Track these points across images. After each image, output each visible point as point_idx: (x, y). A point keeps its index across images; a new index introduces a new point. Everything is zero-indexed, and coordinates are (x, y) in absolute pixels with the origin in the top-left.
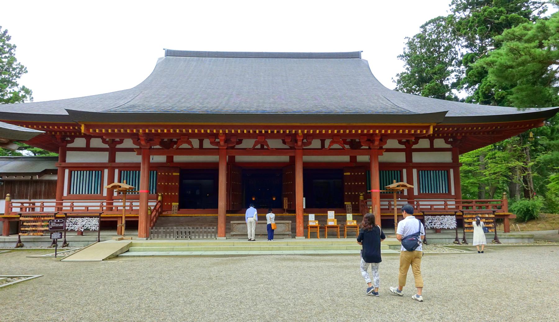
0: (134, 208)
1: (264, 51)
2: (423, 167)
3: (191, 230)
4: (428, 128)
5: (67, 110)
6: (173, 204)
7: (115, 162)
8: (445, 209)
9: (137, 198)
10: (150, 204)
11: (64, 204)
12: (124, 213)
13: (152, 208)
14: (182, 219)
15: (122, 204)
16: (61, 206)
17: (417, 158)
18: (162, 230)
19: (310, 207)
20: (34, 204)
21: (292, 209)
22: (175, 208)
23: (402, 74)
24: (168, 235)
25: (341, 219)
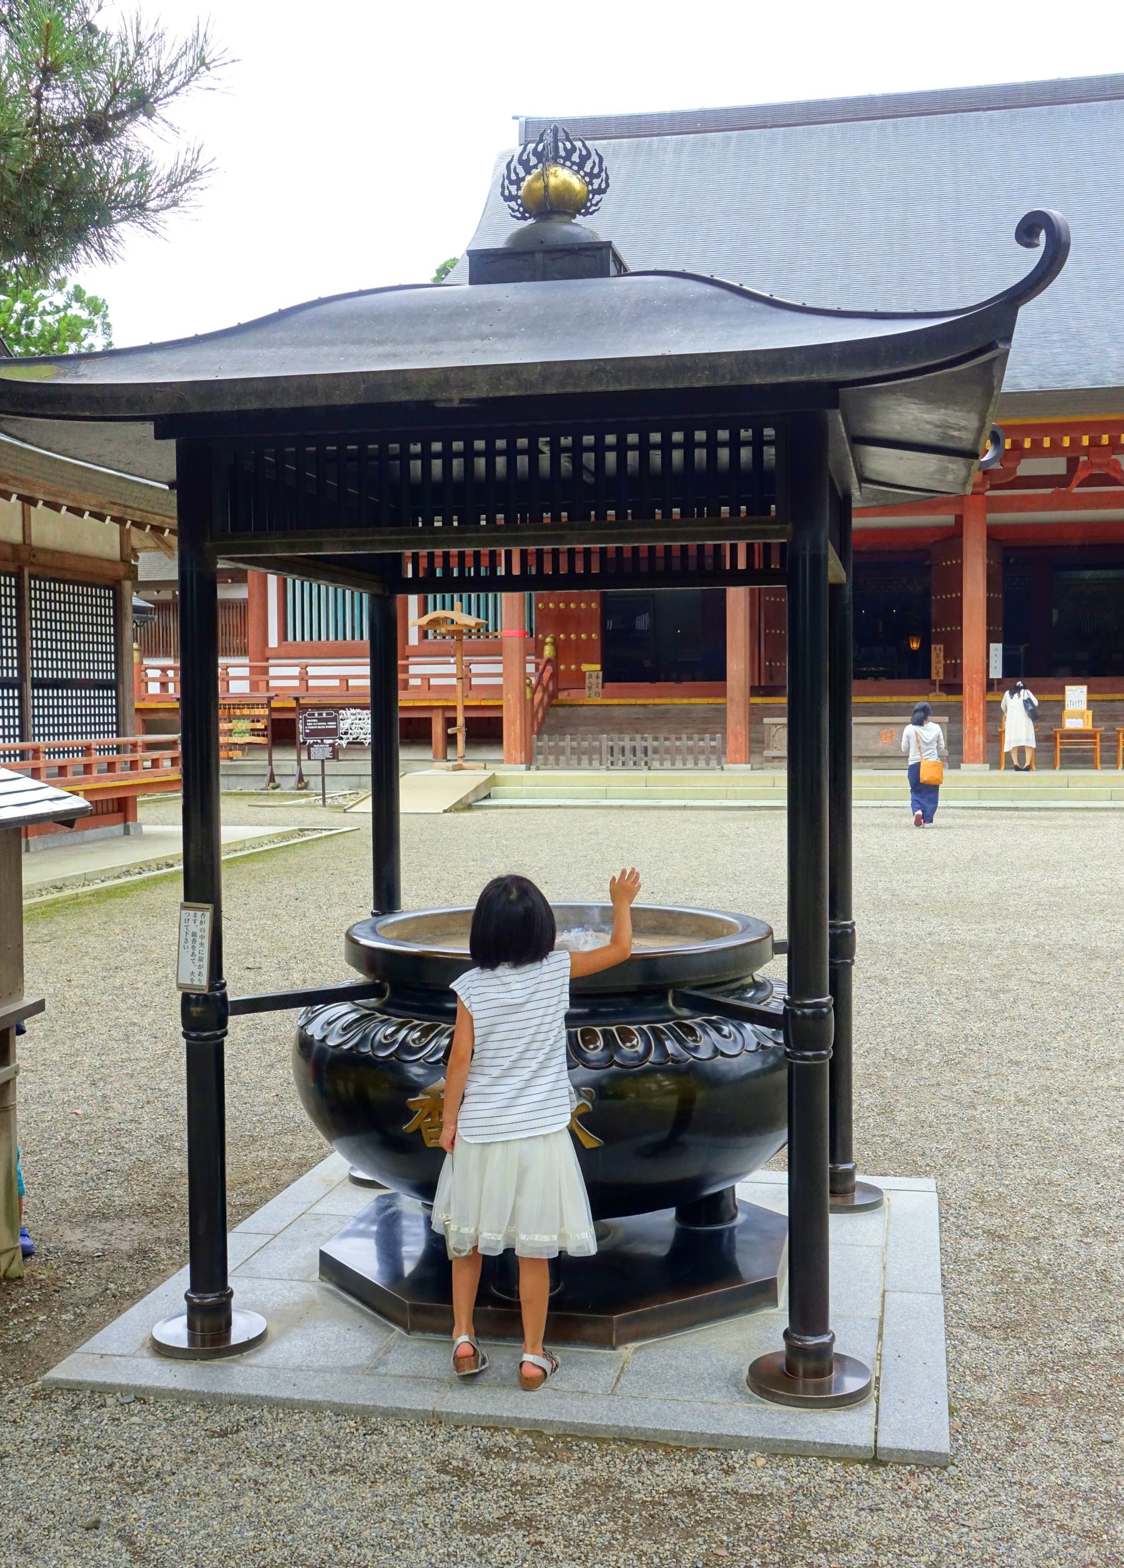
0: (311, 683)
3: (651, 744)
6: (585, 667)
11: (273, 671)
12: (459, 694)
14: (617, 712)
15: (296, 671)
18: (567, 742)
19: (1020, 669)
21: (953, 681)
22: (594, 680)
24: (585, 758)
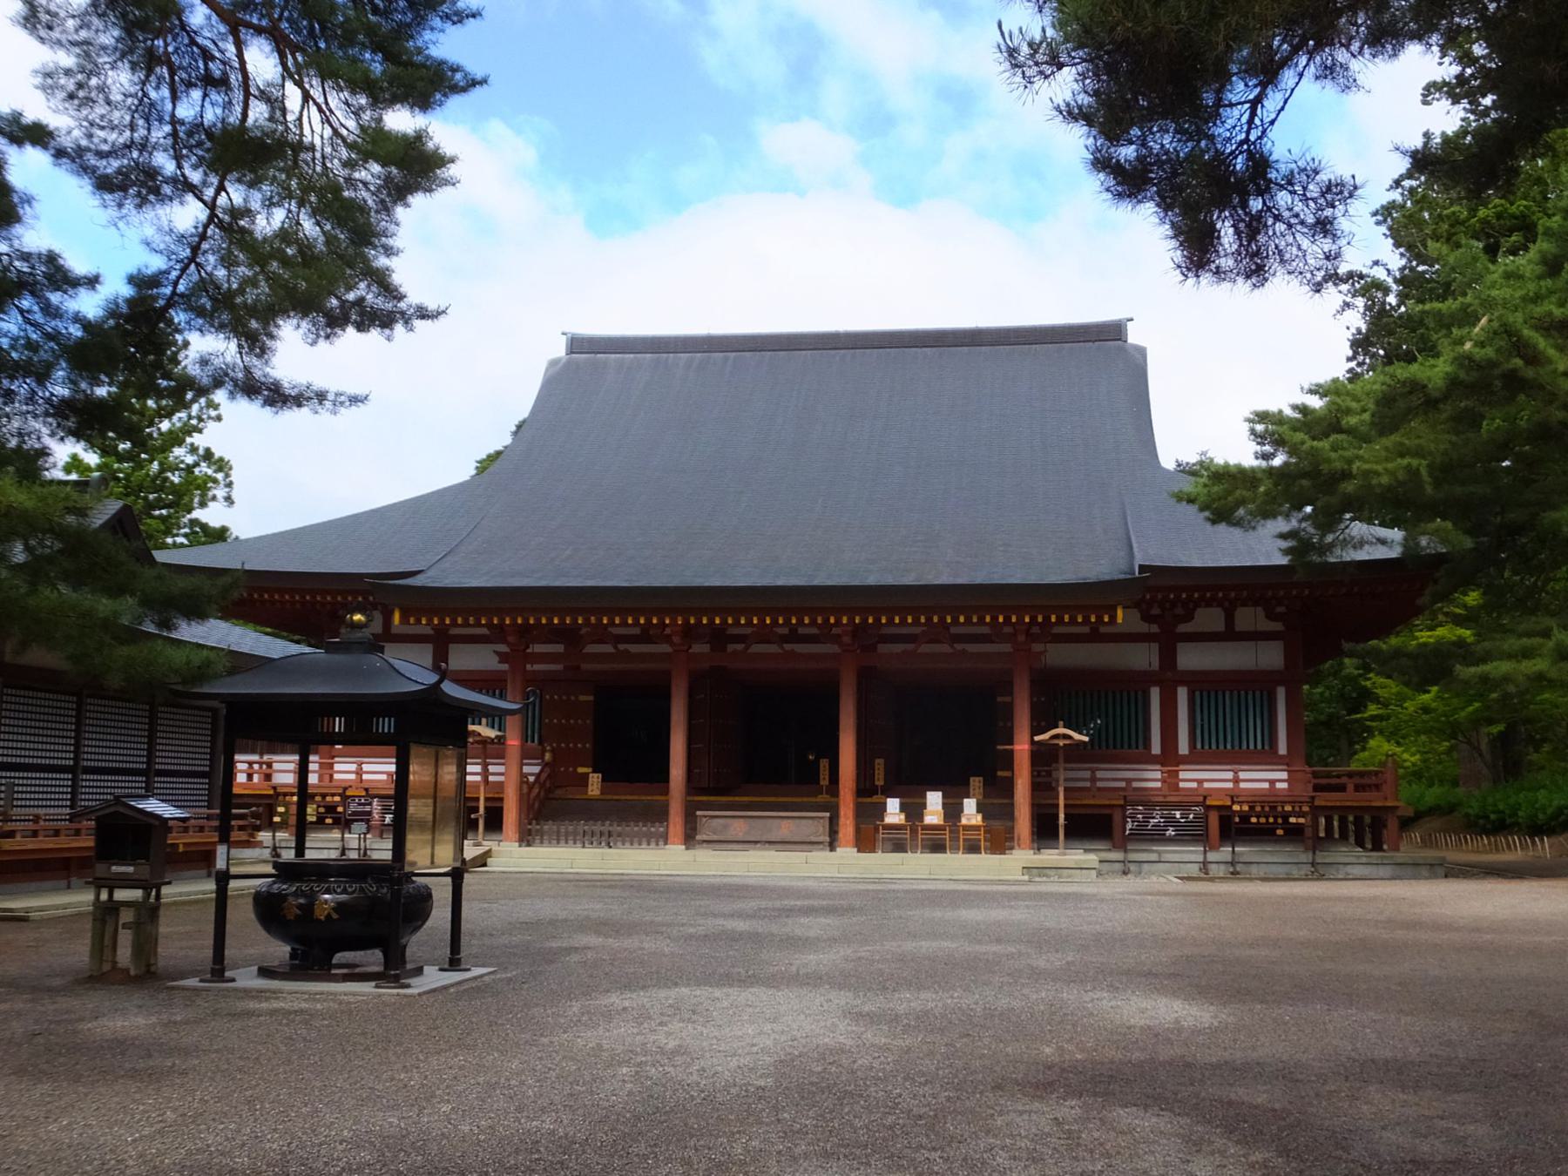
0: (491, 778)
1: (270, 532)
2: (1206, 686)
9: (501, 755)
10: (526, 769)
11: (337, 767)
13: (532, 779)
17: (1191, 658)
20: (269, 765)
25: (952, 811)
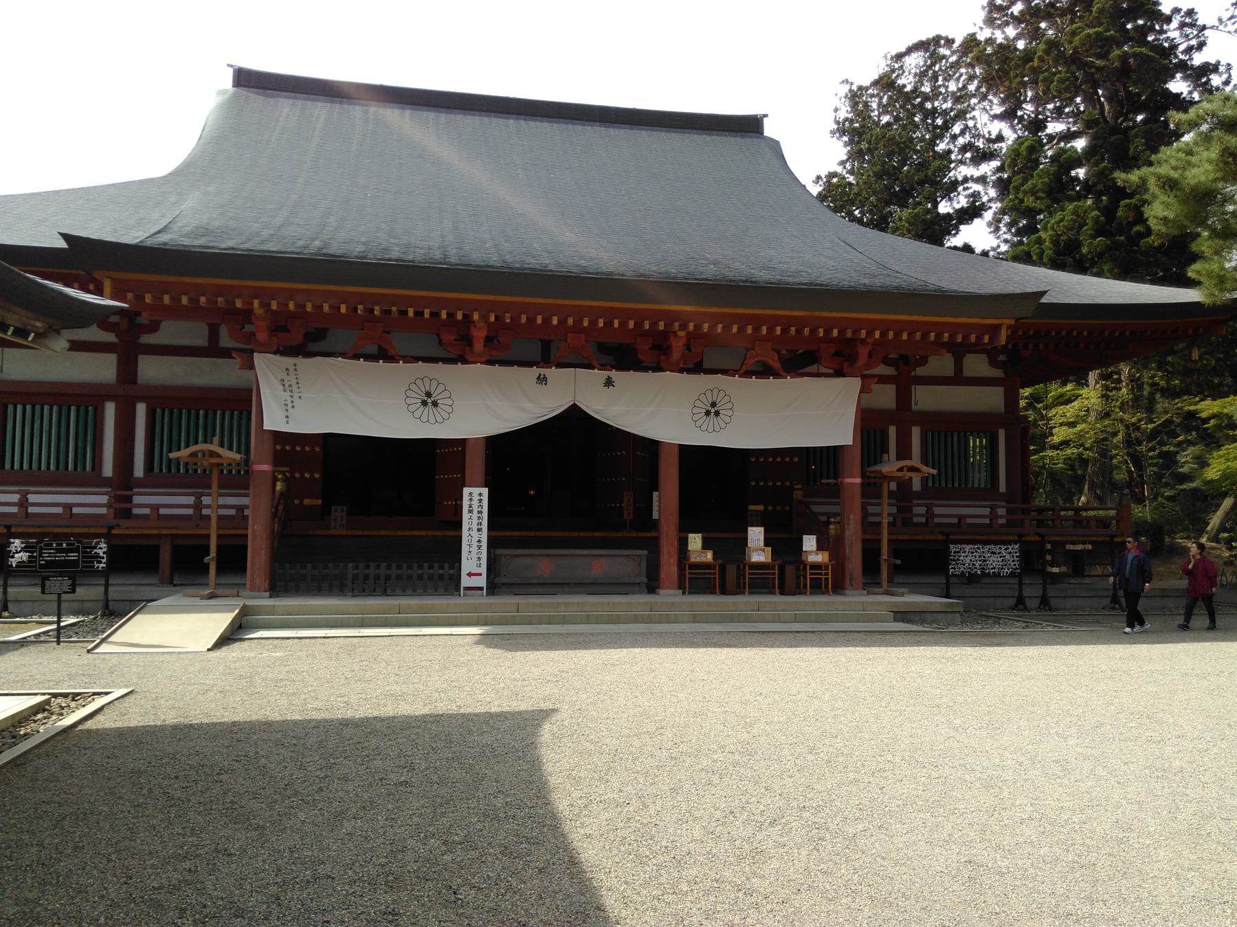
0: (31, 510)
1: (511, 96)
2: (167, 402)
3: (394, 571)
4: (995, 329)
5: (66, 237)
7: (136, 383)
8: (990, 525)
11: (137, 500)
16: (127, 506)
23: (832, 175)
